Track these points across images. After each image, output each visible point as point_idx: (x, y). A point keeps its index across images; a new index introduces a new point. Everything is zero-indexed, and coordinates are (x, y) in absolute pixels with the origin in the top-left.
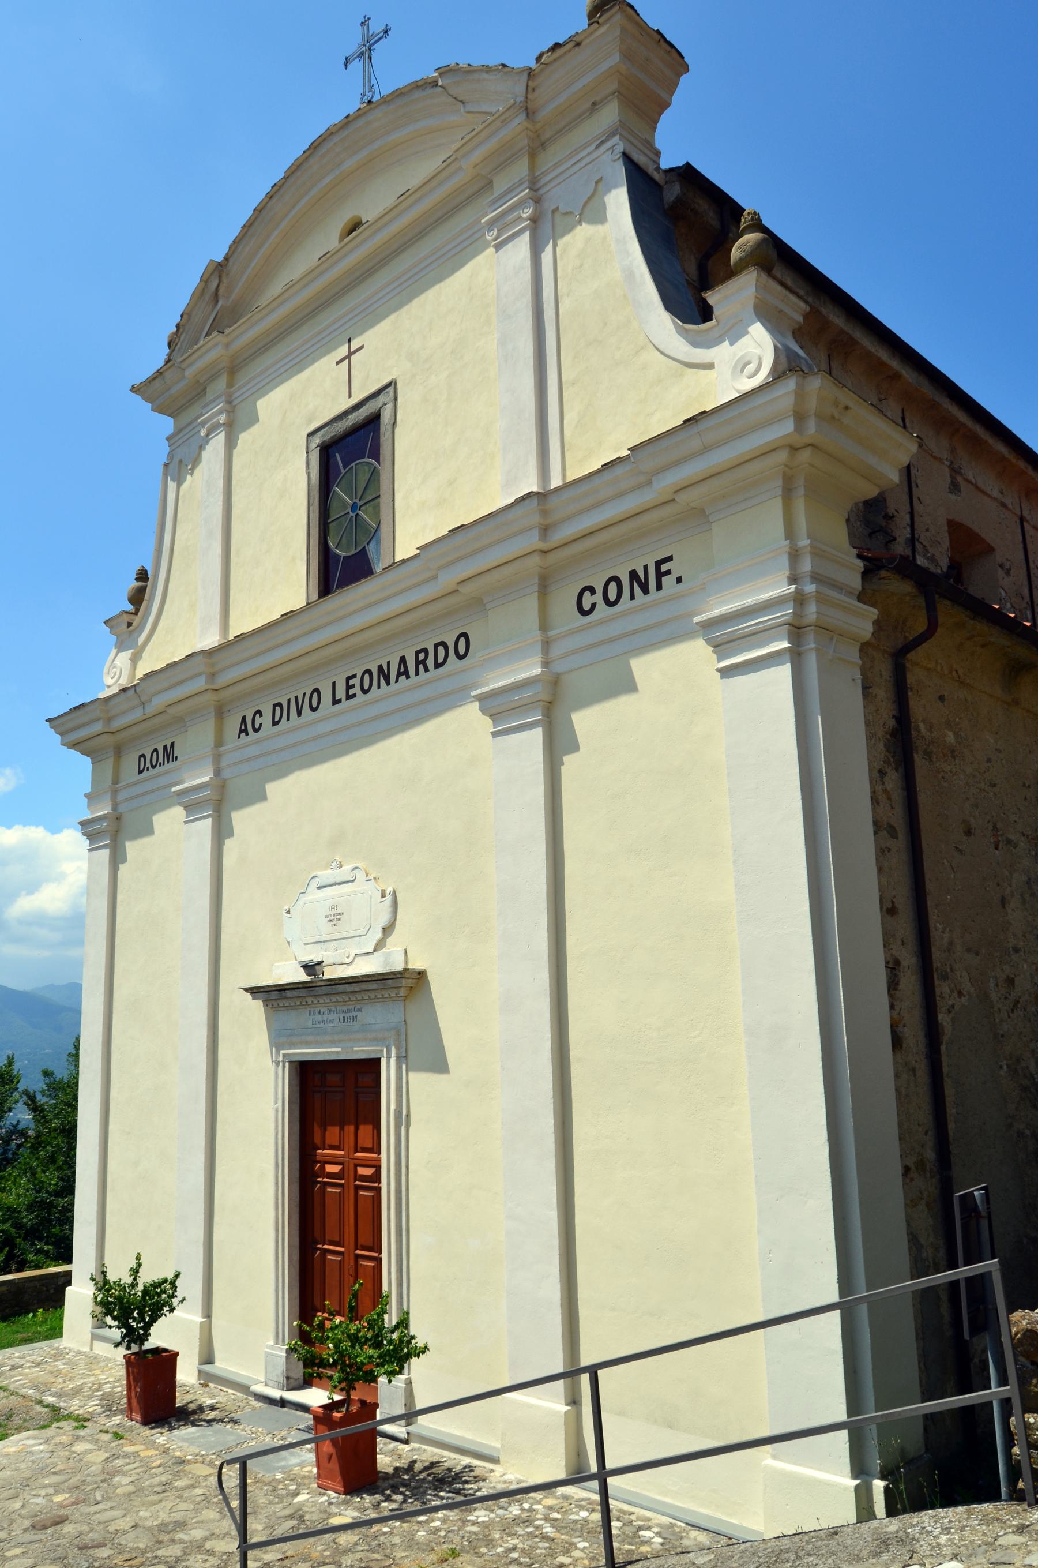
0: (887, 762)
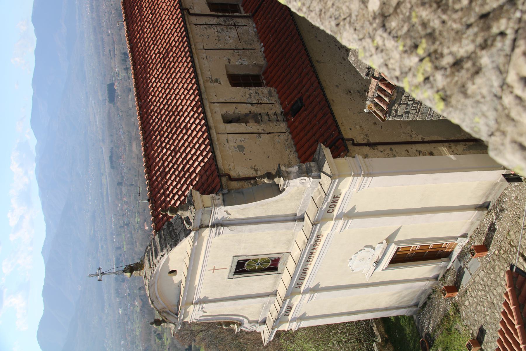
0: (377, 149)
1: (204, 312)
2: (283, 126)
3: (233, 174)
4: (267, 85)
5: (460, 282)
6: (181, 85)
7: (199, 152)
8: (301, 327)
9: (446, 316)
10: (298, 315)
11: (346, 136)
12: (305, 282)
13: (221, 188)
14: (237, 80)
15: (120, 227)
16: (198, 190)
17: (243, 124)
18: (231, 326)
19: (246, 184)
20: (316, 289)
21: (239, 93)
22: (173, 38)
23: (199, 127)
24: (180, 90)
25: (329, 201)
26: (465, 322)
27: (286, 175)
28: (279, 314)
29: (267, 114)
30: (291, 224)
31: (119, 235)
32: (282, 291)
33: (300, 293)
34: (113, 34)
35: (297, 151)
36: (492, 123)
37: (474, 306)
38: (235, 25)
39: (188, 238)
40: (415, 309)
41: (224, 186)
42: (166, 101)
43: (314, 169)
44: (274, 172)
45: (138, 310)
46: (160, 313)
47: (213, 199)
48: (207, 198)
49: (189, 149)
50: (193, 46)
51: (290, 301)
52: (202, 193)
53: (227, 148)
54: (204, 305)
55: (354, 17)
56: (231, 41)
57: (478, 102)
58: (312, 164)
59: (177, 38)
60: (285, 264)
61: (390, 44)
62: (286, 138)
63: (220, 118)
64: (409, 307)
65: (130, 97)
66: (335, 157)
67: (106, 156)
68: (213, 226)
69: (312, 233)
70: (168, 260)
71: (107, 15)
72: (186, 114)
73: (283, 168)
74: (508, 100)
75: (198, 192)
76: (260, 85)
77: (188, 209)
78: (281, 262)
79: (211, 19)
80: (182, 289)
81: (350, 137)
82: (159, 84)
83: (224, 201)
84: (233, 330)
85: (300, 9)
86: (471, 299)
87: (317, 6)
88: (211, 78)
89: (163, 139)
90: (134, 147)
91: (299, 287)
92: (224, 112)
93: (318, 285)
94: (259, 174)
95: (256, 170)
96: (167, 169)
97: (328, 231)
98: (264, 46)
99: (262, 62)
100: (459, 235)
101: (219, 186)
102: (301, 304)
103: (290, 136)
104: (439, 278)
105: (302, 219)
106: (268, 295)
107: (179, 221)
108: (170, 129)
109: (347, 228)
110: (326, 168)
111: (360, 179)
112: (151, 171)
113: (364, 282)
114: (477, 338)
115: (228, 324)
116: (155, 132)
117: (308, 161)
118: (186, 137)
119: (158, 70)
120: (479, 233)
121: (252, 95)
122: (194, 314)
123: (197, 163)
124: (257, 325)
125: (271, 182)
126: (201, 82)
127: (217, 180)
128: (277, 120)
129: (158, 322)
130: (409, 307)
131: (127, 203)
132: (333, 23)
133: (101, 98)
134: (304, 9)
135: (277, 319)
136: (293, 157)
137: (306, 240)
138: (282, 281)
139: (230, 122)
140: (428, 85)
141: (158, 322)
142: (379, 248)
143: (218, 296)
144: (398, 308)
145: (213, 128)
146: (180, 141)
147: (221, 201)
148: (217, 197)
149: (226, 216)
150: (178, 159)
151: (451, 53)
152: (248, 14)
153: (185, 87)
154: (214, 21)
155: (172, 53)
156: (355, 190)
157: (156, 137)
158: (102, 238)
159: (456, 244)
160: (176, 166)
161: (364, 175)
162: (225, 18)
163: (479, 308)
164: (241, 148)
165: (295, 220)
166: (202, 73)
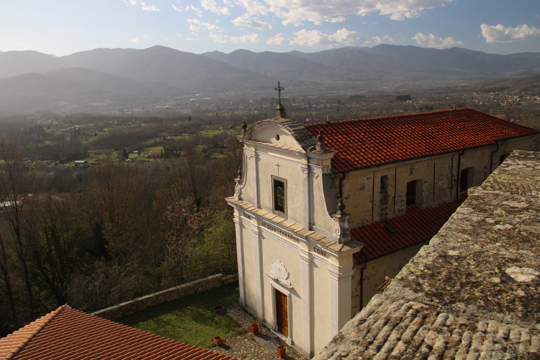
1: (250, 158)
2: (377, 219)
3: (345, 182)
4: (408, 209)
7: (361, 158)
9: (239, 326)
10: (244, 223)
11: (368, 263)
13: (335, 173)
14: (412, 187)
15: (309, 102)
16: (334, 156)
17: (380, 190)
18: (239, 176)
19: (337, 190)
20: (261, 236)
21: (402, 188)
22: (443, 142)
23: (379, 159)
25: (323, 249)
28: (245, 209)
29: (387, 208)
32: (261, 212)
33: (259, 224)
34: (446, 100)
35: (359, 228)
36: (391, 296)
38: (451, 187)
39: (301, 149)
40: (244, 304)
41: (336, 175)
42: (398, 136)
43: (346, 239)
44: (345, 211)
45: (251, 113)
46: (251, 128)
47: (328, 167)
48: (328, 163)
49: (364, 151)
50: (437, 157)
51: (253, 217)
52: (332, 159)
55: (446, 243)
56: (440, 184)
57: (401, 291)
58: (349, 238)
60: (279, 215)
61: (431, 259)
63: (385, 173)
64: (245, 302)
65: (401, 111)
66: (354, 255)
67: (359, 93)
68: (309, 166)
69: (300, 236)
70: (287, 134)
72: (389, 150)
73: (347, 217)
74: (402, 301)
75: (333, 157)
76: (408, 203)
77: (321, 149)
78: (281, 213)
79: (456, 171)
80: (266, 144)
81: (368, 267)
82: (410, 132)
83: (326, 174)
85: (452, 218)
86: (249, 343)
87: (453, 226)
88: (413, 169)
89: (371, 133)
90: (365, 113)
91: (262, 225)
92: (389, 177)
93: (264, 238)
94: (344, 200)
95: (347, 198)
96: (350, 136)
97: (301, 247)
98: (436, 208)
99: (424, 206)
100: (294, 340)
101: (337, 171)
102: (252, 225)
103: (370, 224)
104: (264, 323)
105: (311, 229)
106: (259, 202)
108: (378, 138)
109: (303, 261)
110: (346, 248)
111: (337, 272)
112: (349, 124)
113: (264, 270)
115: (241, 174)
116: (376, 128)
117: (349, 236)
118: (372, 149)
119: (420, 131)
120: (294, 353)
121: (400, 198)
122: (249, 151)
123: (353, 156)
124: (238, 194)
125: (338, 208)
126: (411, 162)
128: (382, 215)
129: (245, 127)
130: (245, 300)
131: (326, 106)
132: (443, 234)
133: (400, 90)
134: (452, 220)
136: (355, 225)
137: (295, 231)
138: (267, 213)
139: (382, 181)
140: (409, 273)
141: (245, 127)
142: (287, 283)
143: (260, 168)
144: (245, 293)
146: (369, 145)
147: (326, 172)
148: (329, 170)
149: (316, 176)
150: (356, 143)
151: (424, 282)
154: (455, 172)
155: (432, 141)
156: (330, 268)
157: (372, 128)
158: (301, 89)
159: (287, 337)
160: (352, 141)
161: (339, 275)
163: (243, 347)
164: (363, 188)
165: (310, 224)
166: (417, 162)
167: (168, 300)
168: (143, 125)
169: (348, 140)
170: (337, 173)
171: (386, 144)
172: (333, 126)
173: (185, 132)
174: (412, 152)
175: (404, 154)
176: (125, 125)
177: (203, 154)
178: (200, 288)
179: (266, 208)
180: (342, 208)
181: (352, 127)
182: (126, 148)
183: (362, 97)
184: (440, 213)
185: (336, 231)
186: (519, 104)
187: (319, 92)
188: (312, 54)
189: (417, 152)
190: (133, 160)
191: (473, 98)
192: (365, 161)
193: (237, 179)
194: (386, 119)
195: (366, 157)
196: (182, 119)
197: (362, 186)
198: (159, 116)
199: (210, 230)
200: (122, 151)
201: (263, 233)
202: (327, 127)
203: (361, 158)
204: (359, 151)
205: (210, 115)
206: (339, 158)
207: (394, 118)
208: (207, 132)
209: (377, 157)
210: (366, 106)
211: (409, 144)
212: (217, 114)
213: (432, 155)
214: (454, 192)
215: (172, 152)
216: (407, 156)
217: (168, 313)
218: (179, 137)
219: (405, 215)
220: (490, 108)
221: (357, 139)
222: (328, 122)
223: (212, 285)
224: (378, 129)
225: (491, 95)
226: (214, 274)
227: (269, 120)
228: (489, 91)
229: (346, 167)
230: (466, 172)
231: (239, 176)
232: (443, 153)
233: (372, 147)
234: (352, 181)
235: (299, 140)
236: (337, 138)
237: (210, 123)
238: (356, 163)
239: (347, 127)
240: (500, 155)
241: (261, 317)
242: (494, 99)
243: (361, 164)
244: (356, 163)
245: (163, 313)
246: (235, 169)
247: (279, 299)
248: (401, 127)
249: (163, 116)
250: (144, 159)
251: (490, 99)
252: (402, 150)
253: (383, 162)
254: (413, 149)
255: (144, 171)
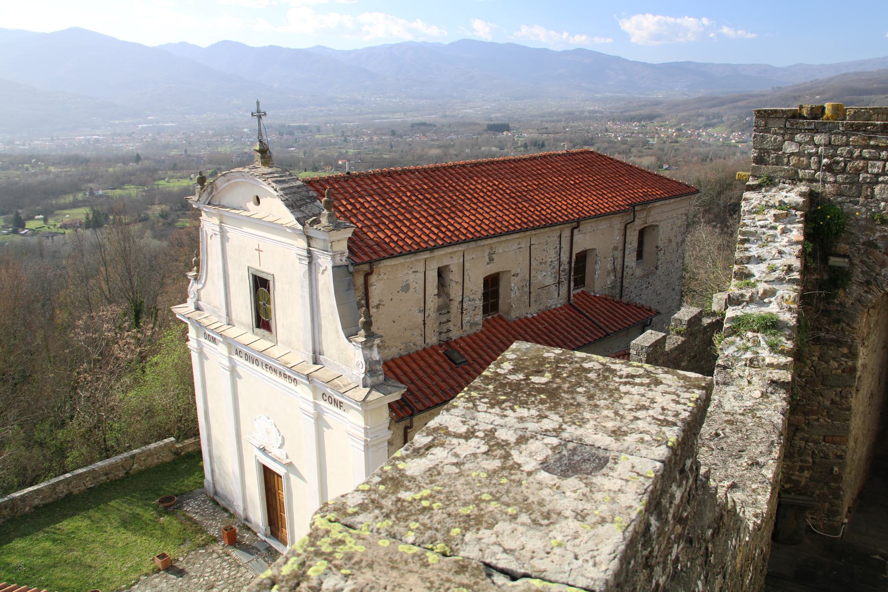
1: (211, 236)
2: (433, 340)
3: (373, 279)
4: (487, 321)
5: (240, 549)
6: (488, 216)
7: (403, 236)
8: (192, 352)
10: (205, 350)
12: (243, 360)
13: (355, 264)
15: (343, 132)
16: (354, 233)
18: (195, 268)
24: (481, 214)
26: (193, 553)
27: (368, 345)
29: (449, 321)
30: (311, 349)
31: (334, 130)
32: (232, 332)
33: (230, 353)
34: (565, 133)
35: (401, 357)
37: (211, 564)
38: (559, 283)
41: (357, 267)
42: (470, 197)
43: (375, 379)
45: (246, 150)
47: (342, 254)
48: (343, 246)
49: (408, 224)
50: (533, 232)
53: (406, 271)
54: (219, 236)
56: (540, 278)
58: (382, 378)
59: (544, 213)
60: (264, 337)
62: (419, 343)
65: (494, 149)
66: (390, 405)
67: (425, 119)
68: (309, 252)
69: (298, 374)
70: (272, 196)
71: (587, 127)
72: (452, 222)
73: (377, 341)
76: (486, 310)
77: (329, 222)
78: (266, 333)
79: (568, 255)
80: (237, 212)
84: (191, 270)
86: (218, 561)
90: (435, 152)
92: (452, 268)
94: (373, 311)
95: (378, 307)
98: (533, 317)
99: (514, 315)
101: (358, 261)
102: (218, 354)
103: (420, 349)
104: (246, 523)
106: (228, 314)
107: (317, 211)
110: (376, 395)
111: (362, 435)
113: (243, 433)
114: (172, 566)
115: (197, 264)
117: (388, 370)
121: (472, 303)
122: (209, 224)
124: (194, 300)
126: (489, 241)
127: (366, 258)
128: (440, 333)
131: (371, 140)
133: (493, 116)
135: (199, 323)
136: (393, 352)
137: (289, 366)
143: (229, 253)
144: (213, 471)
145: (432, 255)
147: (339, 263)
148: (344, 259)
149: (321, 269)
152: (572, 298)
153: (485, 221)
154: (565, 258)
157: (425, 184)
158: (331, 110)
161: (366, 441)
162: (567, 270)
163: (209, 570)
164: (406, 288)
165: (314, 353)
167: (76, 491)
168: (52, 169)
169: (382, 205)
170: (359, 264)
171: (448, 211)
172: (357, 179)
173: (130, 182)
174: (491, 225)
175: (479, 229)
176: (17, 170)
177: (161, 219)
178: (135, 466)
179: (242, 324)
180: (368, 325)
181: (389, 181)
182: (20, 211)
183: (430, 125)
184: (540, 326)
185: (358, 365)
186: (677, 142)
187: (361, 117)
188: (349, 53)
189: (499, 225)
190: (34, 232)
191: (607, 130)
192: (410, 242)
193: (191, 274)
194: (451, 167)
195: (411, 234)
196: (125, 160)
197: (404, 287)
198: (83, 154)
199: (155, 359)
200: (12, 216)
201: (239, 369)
202: (346, 181)
203: (403, 236)
204: (399, 224)
205: (174, 152)
206: (363, 236)
207: (463, 166)
208: (168, 182)
209: (431, 235)
210: (438, 140)
211: (488, 210)
212: (186, 151)
213: (527, 230)
214: (564, 289)
215: (107, 218)
216: (483, 232)
217: (73, 515)
218: (118, 192)
219: (482, 332)
220: (632, 146)
221: (397, 203)
222: (348, 173)
223: (158, 458)
224: (435, 185)
225: (635, 126)
226: (161, 437)
227: (241, 169)
228: (632, 119)
229: (375, 252)
230: (582, 257)
231: (195, 268)
232: (545, 227)
233: (424, 217)
234: (386, 277)
235: (292, 206)
236: (362, 201)
237: (175, 168)
238: (392, 245)
239: (382, 182)
240: (638, 228)
241: (240, 511)
242: (639, 133)
243: (402, 247)
244: (392, 245)
245: (65, 517)
246: (186, 255)
247: (270, 479)
248: (476, 181)
249: (89, 154)
250: (55, 230)
251: (633, 133)
252: (474, 221)
253: (440, 242)
254: (493, 220)
255: (55, 252)
